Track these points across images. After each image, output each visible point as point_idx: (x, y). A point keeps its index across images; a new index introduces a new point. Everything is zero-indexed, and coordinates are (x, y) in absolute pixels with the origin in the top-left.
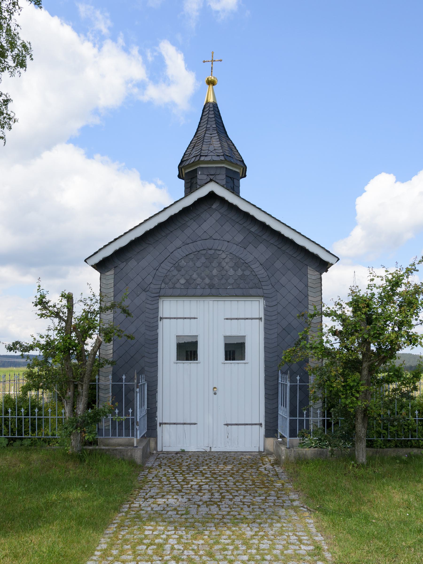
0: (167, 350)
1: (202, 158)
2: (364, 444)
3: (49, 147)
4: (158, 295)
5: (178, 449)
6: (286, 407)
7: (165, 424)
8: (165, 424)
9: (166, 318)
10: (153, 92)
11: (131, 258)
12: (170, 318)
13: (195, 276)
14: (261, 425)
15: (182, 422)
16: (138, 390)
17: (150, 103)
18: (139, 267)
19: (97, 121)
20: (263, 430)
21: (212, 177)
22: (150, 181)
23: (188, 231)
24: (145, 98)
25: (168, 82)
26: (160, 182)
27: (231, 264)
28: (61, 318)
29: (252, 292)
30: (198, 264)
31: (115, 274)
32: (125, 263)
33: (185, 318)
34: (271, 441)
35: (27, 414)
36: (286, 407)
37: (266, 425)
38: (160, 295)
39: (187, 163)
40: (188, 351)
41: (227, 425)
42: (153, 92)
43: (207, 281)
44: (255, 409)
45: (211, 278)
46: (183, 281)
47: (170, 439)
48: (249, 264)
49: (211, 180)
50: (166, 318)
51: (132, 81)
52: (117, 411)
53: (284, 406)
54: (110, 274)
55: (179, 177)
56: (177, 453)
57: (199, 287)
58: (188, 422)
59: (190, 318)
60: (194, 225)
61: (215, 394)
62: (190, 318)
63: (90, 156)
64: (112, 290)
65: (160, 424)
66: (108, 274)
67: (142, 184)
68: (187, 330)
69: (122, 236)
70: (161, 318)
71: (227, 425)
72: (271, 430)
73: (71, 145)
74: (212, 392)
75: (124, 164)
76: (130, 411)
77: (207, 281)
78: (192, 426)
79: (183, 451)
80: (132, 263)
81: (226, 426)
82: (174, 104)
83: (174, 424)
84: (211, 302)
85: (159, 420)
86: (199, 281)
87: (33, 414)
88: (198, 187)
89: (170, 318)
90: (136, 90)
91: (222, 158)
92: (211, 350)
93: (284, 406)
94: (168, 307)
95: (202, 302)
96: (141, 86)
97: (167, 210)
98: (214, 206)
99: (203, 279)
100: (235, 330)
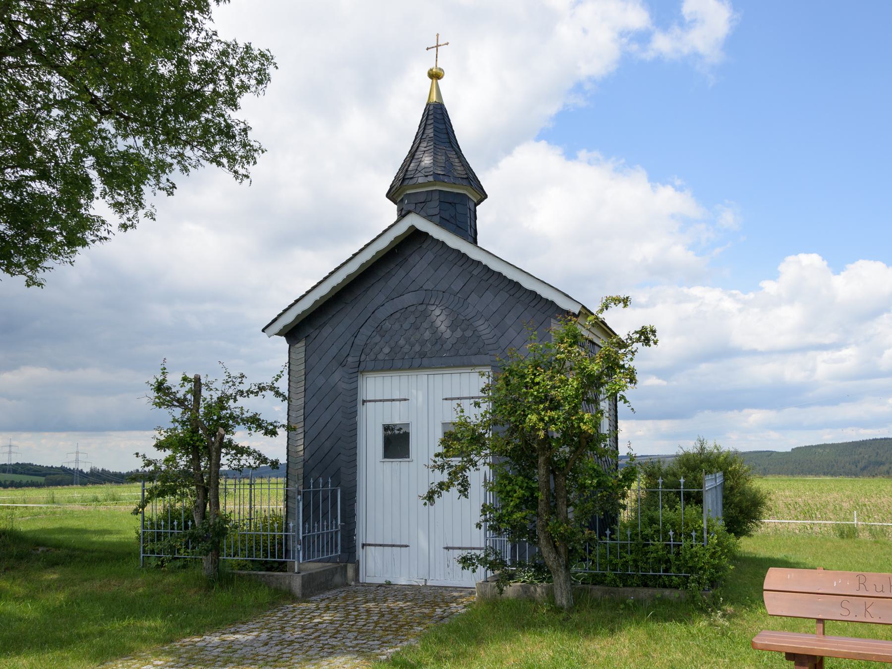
0: (371, 442)
2: (562, 578)
3: (508, 151)
4: (356, 370)
5: (382, 581)
7: (369, 545)
8: (369, 545)
9: (370, 401)
10: (662, 44)
11: (325, 324)
12: (375, 401)
13: (402, 342)
16: (299, 497)
17: (659, 60)
18: (334, 332)
19: (581, 102)
22: (664, 184)
23: (393, 282)
24: (649, 56)
25: (685, 25)
26: (678, 182)
27: (447, 323)
28: (186, 408)
29: (474, 360)
30: (406, 326)
31: (306, 346)
32: (318, 331)
33: (394, 400)
38: (361, 369)
40: (396, 443)
41: (447, 548)
42: (662, 44)
45: (423, 343)
46: (386, 350)
48: (471, 321)
50: (370, 401)
51: (629, 33)
54: (301, 346)
56: (381, 585)
57: (407, 357)
58: (398, 543)
60: (401, 273)
63: (570, 155)
64: (303, 366)
65: (364, 545)
66: (298, 346)
67: (652, 186)
68: (396, 416)
69: (303, 296)
70: (364, 402)
71: (447, 548)
73: (543, 143)
75: (623, 161)
77: (417, 348)
79: (389, 584)
80: (326, 331)
81: (446, 551)
82: (697, 56)
83: (380, 545)
85: (360, 539)
86: (407, 348)
89: (375, 401)
90: (635, 47)
91: (431, 179)
94: (374, 386)
96: (643, 38)
97: (358, 256)
99: (412, 346)
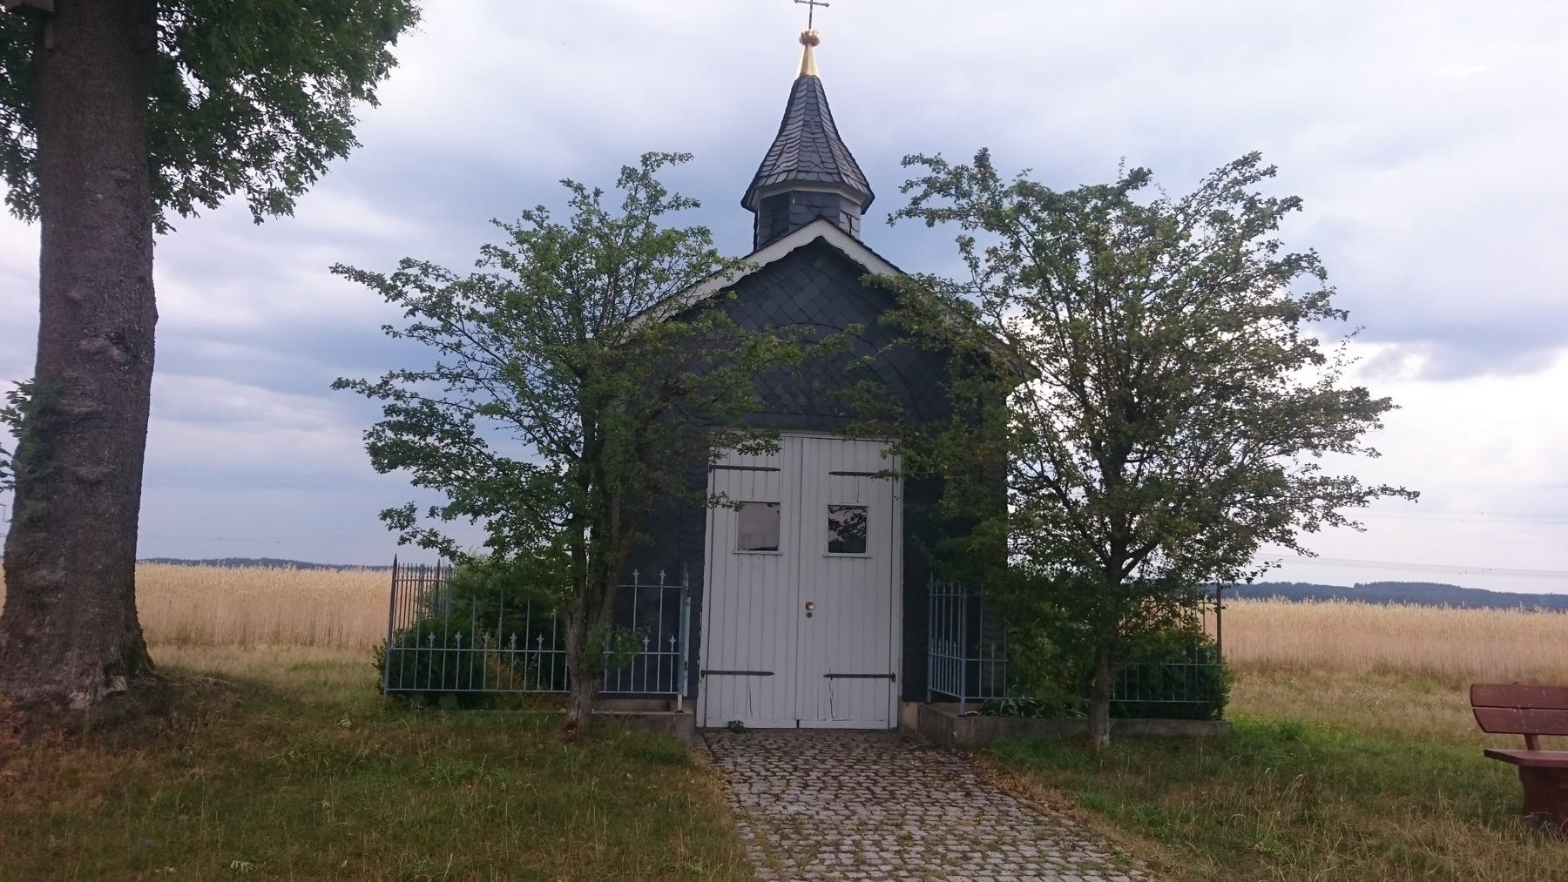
1: (802, 176)
6: (955, 639)
14: (892, 677)
15: (745, 669)
20: (896, 689)
21: (816, 211)
34: (912, 709)
35: (438, 643)
36: (955, 639)
37: (904, 679)
39: (771, 181)
41: (831, 676)
43: (802, 400)
44: (883, 646)
47: (721, 702)
49: (819, 218)
52: (646, 641)
53: (947, 637)
55: (744, 203)
59: (766, 470)
61: (809, 615)
62: (766, 470)
65: (704, 673)
71: (831, 676)
72: (914, 685)
74: (804, 612)
76: (673, 640)
77: (802, 400)
78: (765, 678)
84: (806, 441)
87: (451, 642)
88: (791, 228)
92: (806, 532)
93: (947, 637)
95: (825, 443)
98: (818, 264)
100: (845, 492)
